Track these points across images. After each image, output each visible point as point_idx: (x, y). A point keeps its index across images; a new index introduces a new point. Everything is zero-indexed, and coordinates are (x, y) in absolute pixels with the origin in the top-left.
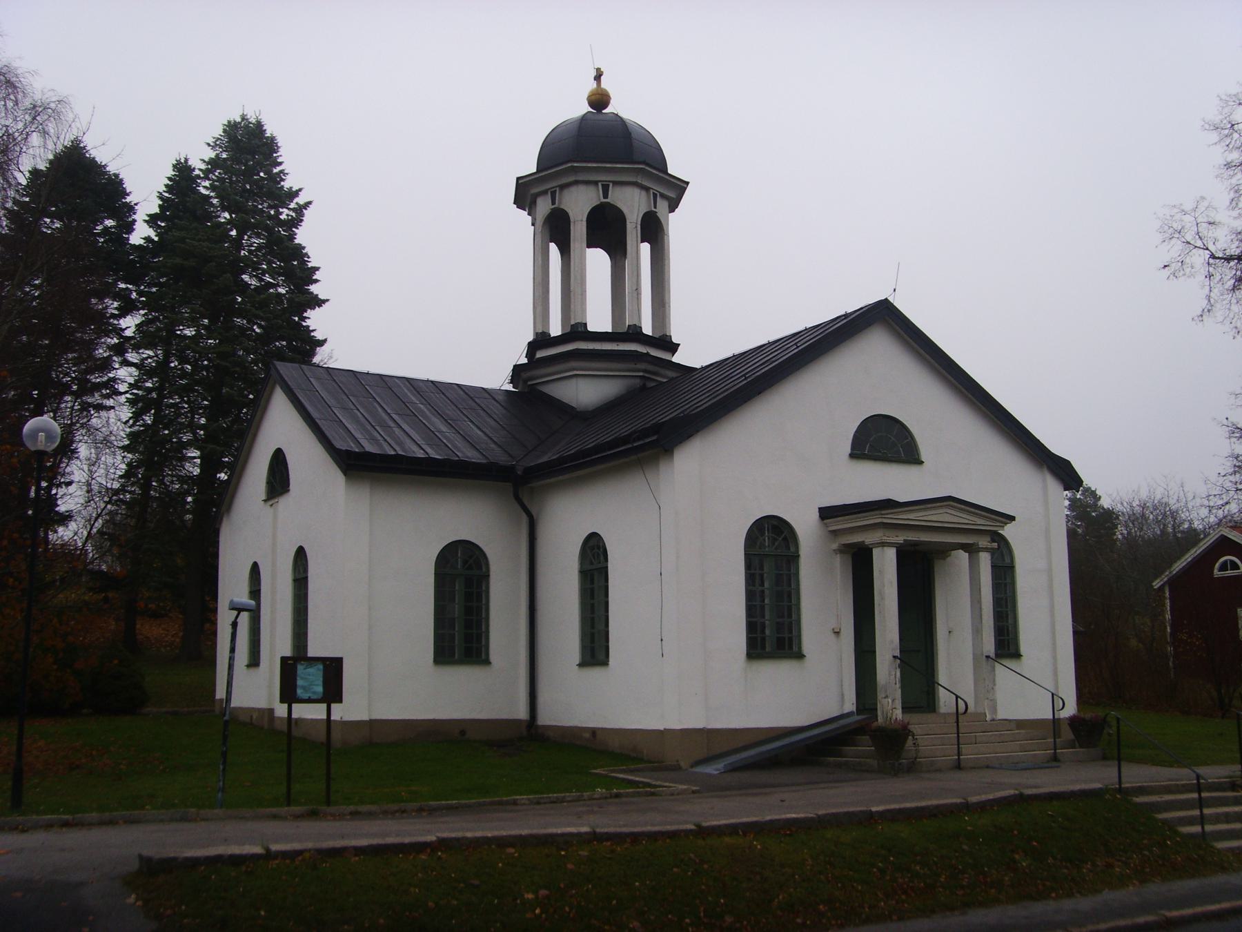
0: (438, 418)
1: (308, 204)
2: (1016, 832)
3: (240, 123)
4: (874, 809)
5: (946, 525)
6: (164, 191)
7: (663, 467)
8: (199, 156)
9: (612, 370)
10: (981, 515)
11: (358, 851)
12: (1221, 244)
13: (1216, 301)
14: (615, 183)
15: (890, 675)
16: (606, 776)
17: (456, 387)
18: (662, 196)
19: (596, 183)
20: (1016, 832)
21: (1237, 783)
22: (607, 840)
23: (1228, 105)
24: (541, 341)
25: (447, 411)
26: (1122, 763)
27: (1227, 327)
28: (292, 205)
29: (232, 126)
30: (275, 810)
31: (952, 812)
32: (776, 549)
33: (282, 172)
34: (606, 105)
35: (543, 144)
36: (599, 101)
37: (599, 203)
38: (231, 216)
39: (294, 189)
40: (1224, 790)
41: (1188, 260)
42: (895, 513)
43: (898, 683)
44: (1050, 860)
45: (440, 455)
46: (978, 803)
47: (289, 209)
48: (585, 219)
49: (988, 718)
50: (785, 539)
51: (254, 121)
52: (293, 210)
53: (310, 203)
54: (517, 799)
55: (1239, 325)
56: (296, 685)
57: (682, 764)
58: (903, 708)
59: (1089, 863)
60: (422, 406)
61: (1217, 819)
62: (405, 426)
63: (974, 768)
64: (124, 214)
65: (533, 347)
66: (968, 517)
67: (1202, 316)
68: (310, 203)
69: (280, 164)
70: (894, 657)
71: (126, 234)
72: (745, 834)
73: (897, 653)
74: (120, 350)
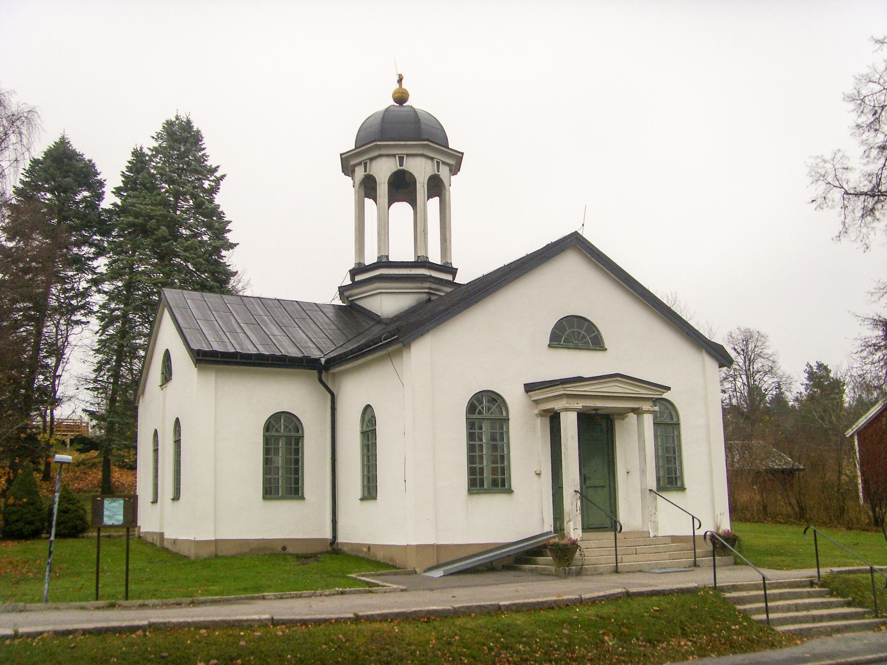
0: (276, 326)
1: (224, 176)
2: (613, 620)
3: (175, 122)
4: (502, 603)
5: (587, 393)
6: (126, 171)
7: (405, 355)
8: (148, 144)
9: (405, 289)
10: (645, 388)
11: (85, 632)
12: (852, 184)
13: (849, 226)
14: (408, 155)
15: (572, 504)
16: (355, 579)
17: (295, 303)
18: (444, 163)
19: (394, 156)
20: (613, 620)
21: (814, 581)
22: (283, 624)
23: (861, 82)
24: (359, 269)
25: (284, 321)
26: (717, 569)
27: (859, 244)
28: (212, 178)
29: (169, 124)
30: (83, 604)
31: (567, 605)
32: (492, 413)
33: (204, 155)
34: (406, 100)
35: (359, 129)
36: (401, 98)
37: (396, 170)
38: (170, 187)
39: (213, 167)
40: (804, 587)
41: (829, 196)
42: (575, 386)
43: (578, 510)
44: (634, 641)
45: (268, 351)
46: (589, 599)
47: (209, 180)
48: (387, 182)
49: (651, 535)
50: (499, 406)
51: (185, 120)
52: (212, 181)
53: (224, 176)
54: (266, 595)
55: (867, 242)
56: (103, 514)
57: (417, 570)
58: (583, 529)
59: (665, 643)
60: (265, 317)
61: (777, 609)
62: (249, 333)
63: (630, 572)
64: (96, 188)
65: (353, 273)
66: (633, 389)
67: (839, 237)
68: (224, 176)
69: (204, 149)
70: (575, 491)
71: (98, 201)
72: (392, 621)
73: (578, 489)
74: (96, 282)
